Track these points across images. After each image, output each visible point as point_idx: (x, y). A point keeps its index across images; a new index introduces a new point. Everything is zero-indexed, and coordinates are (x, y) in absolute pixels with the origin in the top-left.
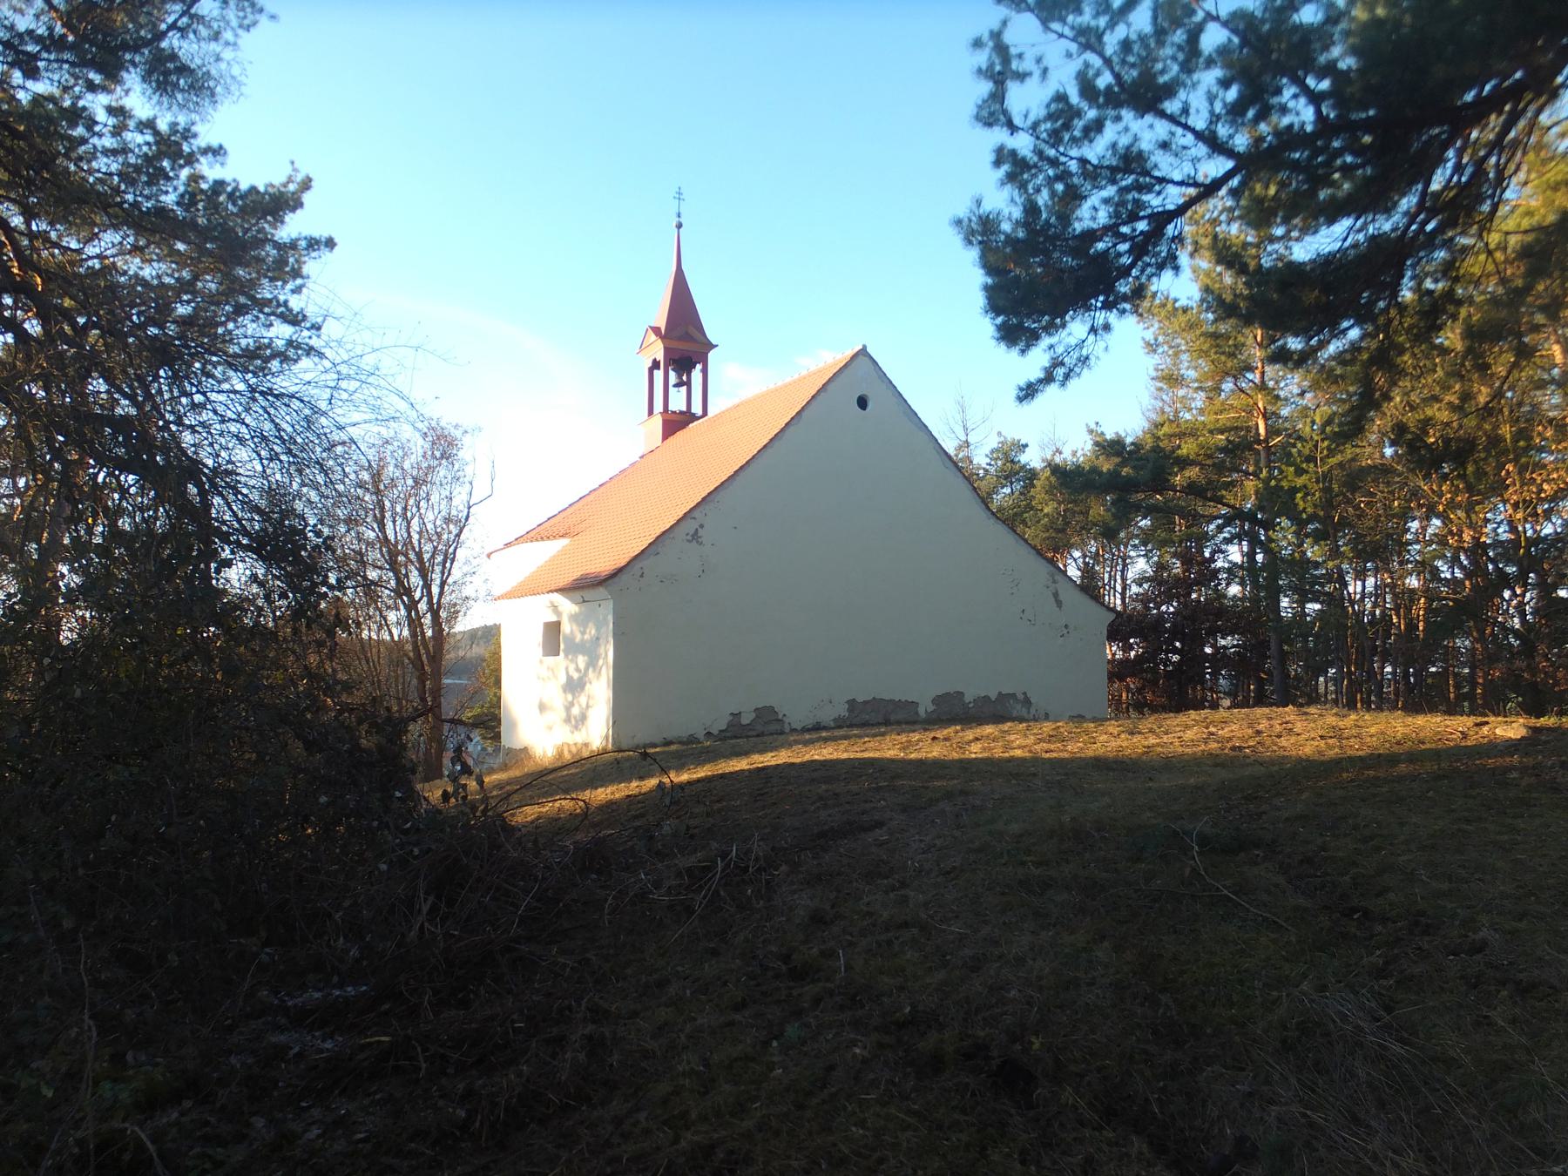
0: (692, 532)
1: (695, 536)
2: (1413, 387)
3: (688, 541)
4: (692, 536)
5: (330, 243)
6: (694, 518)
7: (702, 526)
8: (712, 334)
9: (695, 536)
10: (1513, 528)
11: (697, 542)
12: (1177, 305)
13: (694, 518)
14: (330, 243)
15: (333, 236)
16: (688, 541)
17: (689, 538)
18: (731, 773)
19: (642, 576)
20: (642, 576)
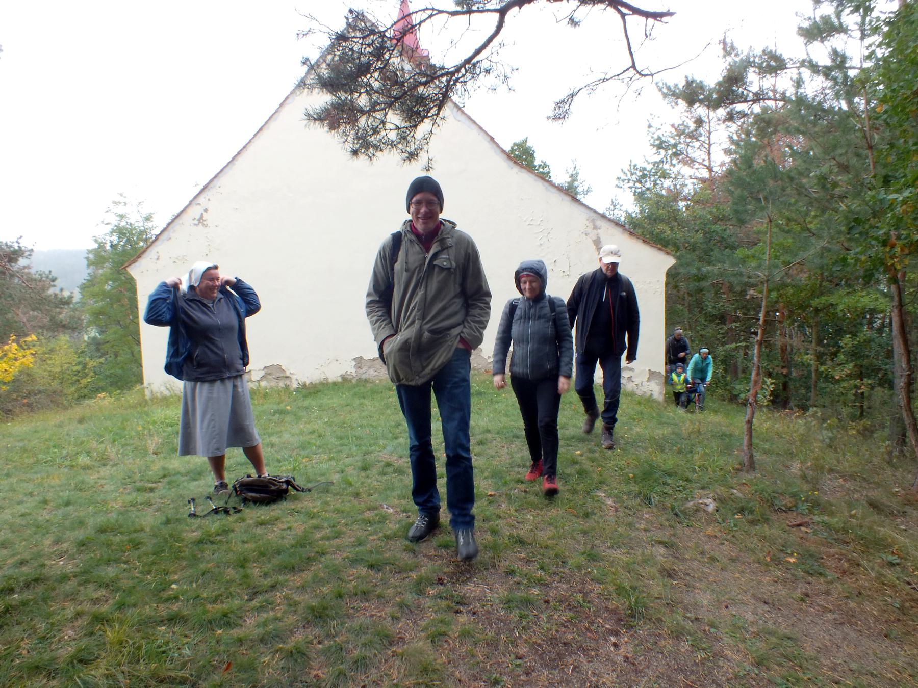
0: (198, 217)
1: (201, 220)
2: (420, 592)
3: (195, 225)
4: (199, 220)
5: (669, 14)
6: (200, 204)
7: (206, 210)
8: (637, 356)
9: (201, 220)
10: (738, 136)
11: (203, 225)
12: (859, 326)
13: (200, 204)
14: (669, 14)
15: (549, 268)
16: (195, 225)
17: (196, 222)
18: (447, 447)
19: (158, 259)
20: (158, 259)
